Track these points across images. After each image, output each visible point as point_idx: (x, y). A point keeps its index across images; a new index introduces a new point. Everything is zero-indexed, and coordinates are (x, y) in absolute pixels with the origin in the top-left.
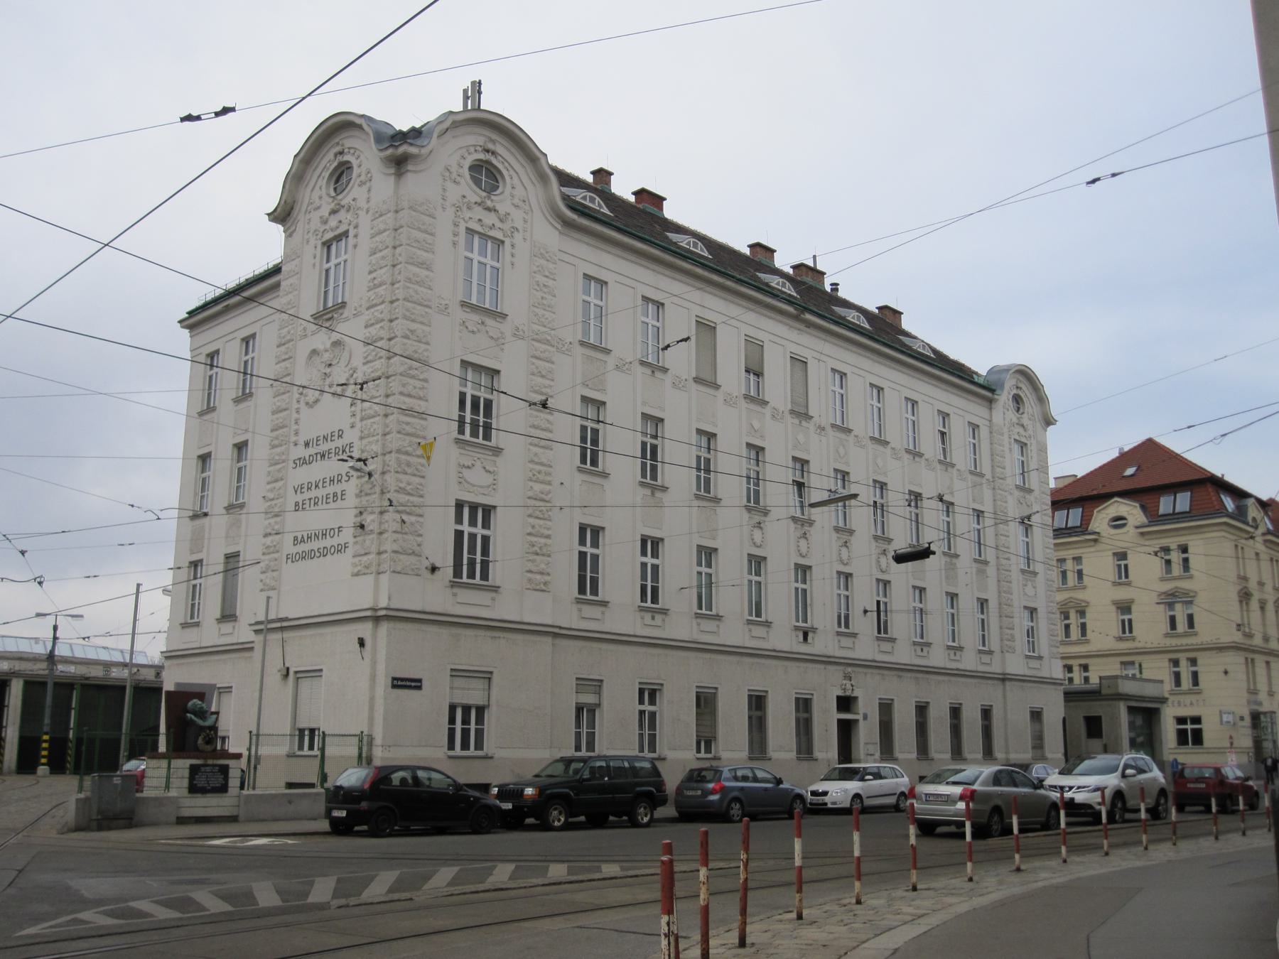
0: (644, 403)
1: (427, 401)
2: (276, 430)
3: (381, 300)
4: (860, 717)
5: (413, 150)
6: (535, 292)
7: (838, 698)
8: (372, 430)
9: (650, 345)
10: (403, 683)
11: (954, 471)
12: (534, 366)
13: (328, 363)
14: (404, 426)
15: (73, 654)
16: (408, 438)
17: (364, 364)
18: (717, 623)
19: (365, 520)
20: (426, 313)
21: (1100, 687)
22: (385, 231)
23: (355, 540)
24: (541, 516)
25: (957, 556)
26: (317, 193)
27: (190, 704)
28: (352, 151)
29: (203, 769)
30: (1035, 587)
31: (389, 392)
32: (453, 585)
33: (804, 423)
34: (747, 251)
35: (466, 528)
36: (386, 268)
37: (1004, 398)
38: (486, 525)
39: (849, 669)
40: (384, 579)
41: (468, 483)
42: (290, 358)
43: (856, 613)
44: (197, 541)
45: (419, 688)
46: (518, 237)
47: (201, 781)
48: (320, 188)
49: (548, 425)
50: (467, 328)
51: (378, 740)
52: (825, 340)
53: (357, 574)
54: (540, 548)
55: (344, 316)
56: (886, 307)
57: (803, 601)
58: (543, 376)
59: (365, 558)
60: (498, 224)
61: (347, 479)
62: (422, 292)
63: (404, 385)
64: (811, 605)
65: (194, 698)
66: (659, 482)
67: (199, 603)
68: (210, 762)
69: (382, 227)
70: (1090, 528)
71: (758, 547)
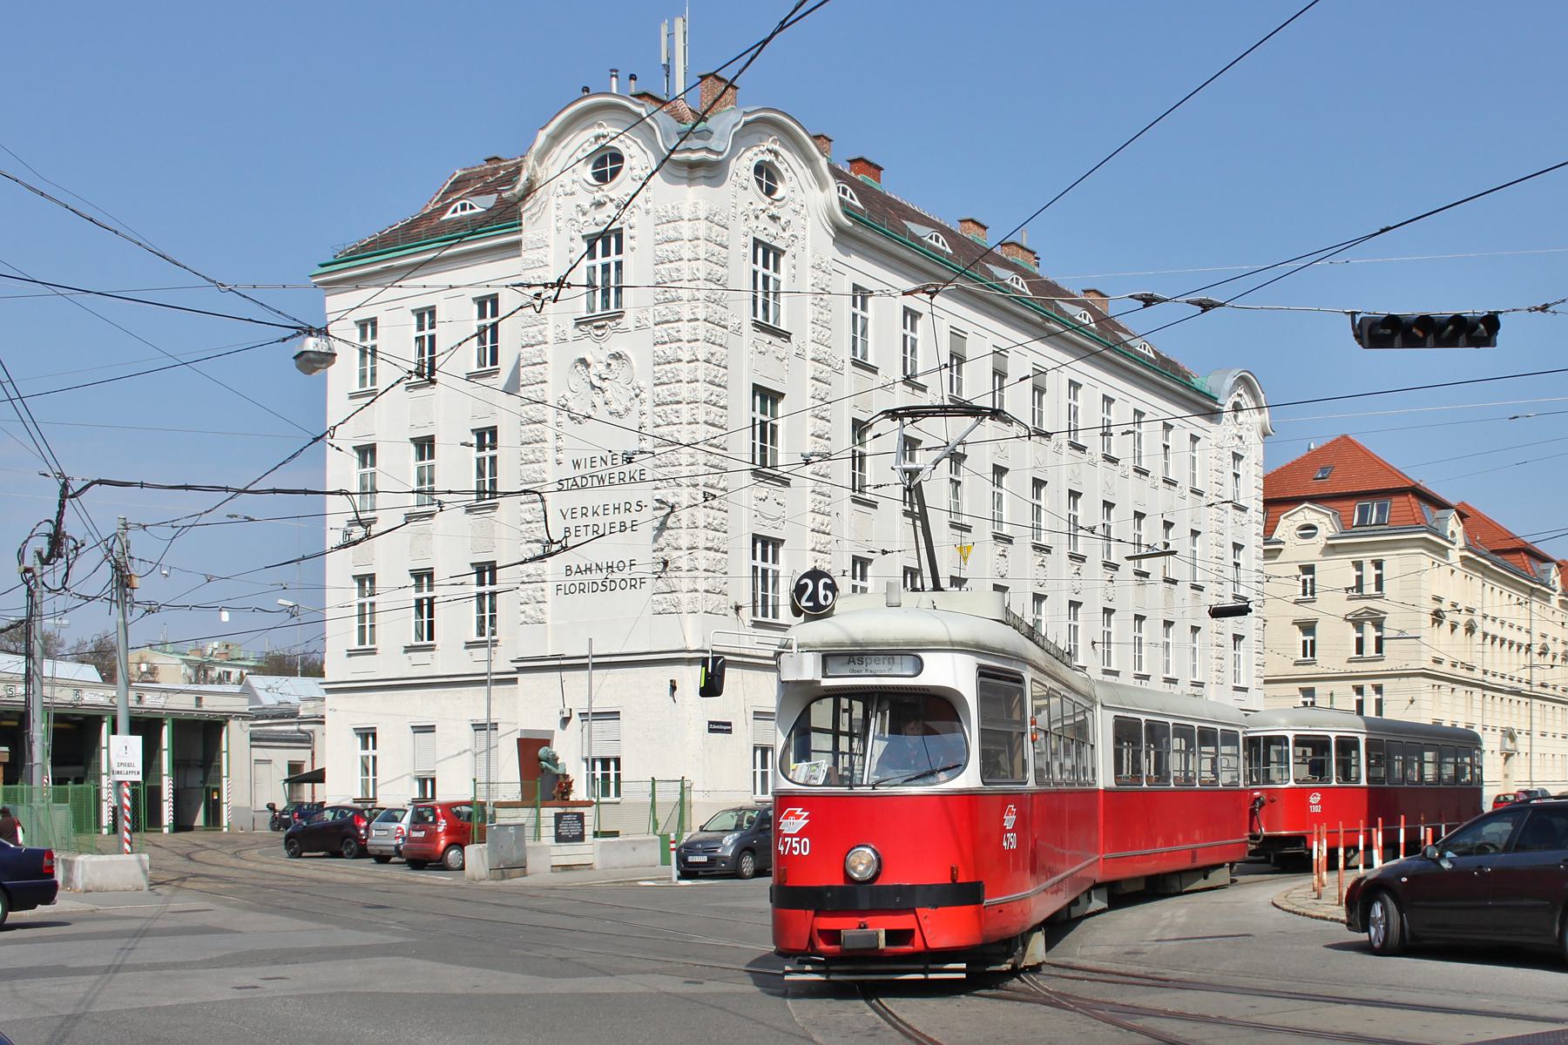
7: (518, 739)
10: (718, 727)
24: (822, 549)
45: (729, 731)
69: (672, 234)
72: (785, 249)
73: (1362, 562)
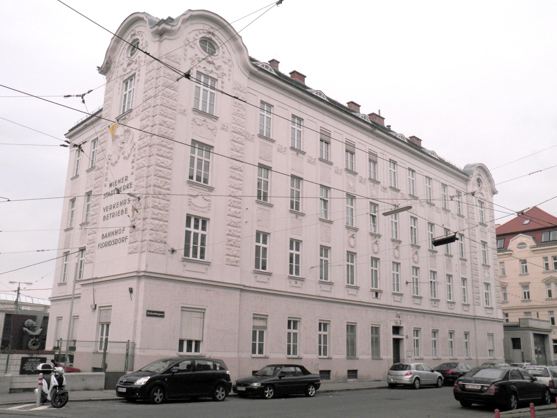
0: (292, 169)
1: (172, 159)
2: (97, 179)
3: (149, 106)
4: (404, 337)
5: (168, 27)
6: (234, 107)
8: (141, 175)
9: (296, 141)
10: (154, 314)
11: (450, 214)
12: (233, 146)
13: (123, 141)
14: (159, 172)
15: (33, 301)
16: (160, 179)
17: (139, 140)
18: (331, 286)
19: (135, 223)
20: (173, 113)
21: (519, 323)
22: (152, 70)
23: (131, 234)
24: (235, 225)
25: (452, 256)
26: (122, 56)
27: (26, 322)
28: (139, 33)
29: (30, 360)
30: (489, 273)
31: (151, 154)
32: (184, 260)
33: (376, 185)
34: (347, 105)
35: (192, 229)
36: (152, 89)
37: (473, 179)
38: (204, 229)
39: (399, 312)
40: (144, 255)
41: (194, 205)
42: (105, 141)
43: (402, 282)
44: (67, 242)
45: (163, 316)
46: (225, 79)
47: (28, 367)
48: (124, 54)
49: (240, 177)
50: (196, 122)
51: (138, 346)
52: (386, 144)
53: (130, 253)
54: (234, 242)
55: (131, 117)
56: (414, 137)
57: (375, 275)
58: (237, 151)
59: (135, 244)
60: (214, 70)
61: (128, 202)
62: (171, 102)
63: (158, 150)
64: (379, 278)
65: (30, 318)
66: (300, 211)
67: (414, 347)
68: (34, 356)
69: (151, 68)
70: (508, 248)
71: (352, 247)
72: (217, 78)
73: (547, 257)
